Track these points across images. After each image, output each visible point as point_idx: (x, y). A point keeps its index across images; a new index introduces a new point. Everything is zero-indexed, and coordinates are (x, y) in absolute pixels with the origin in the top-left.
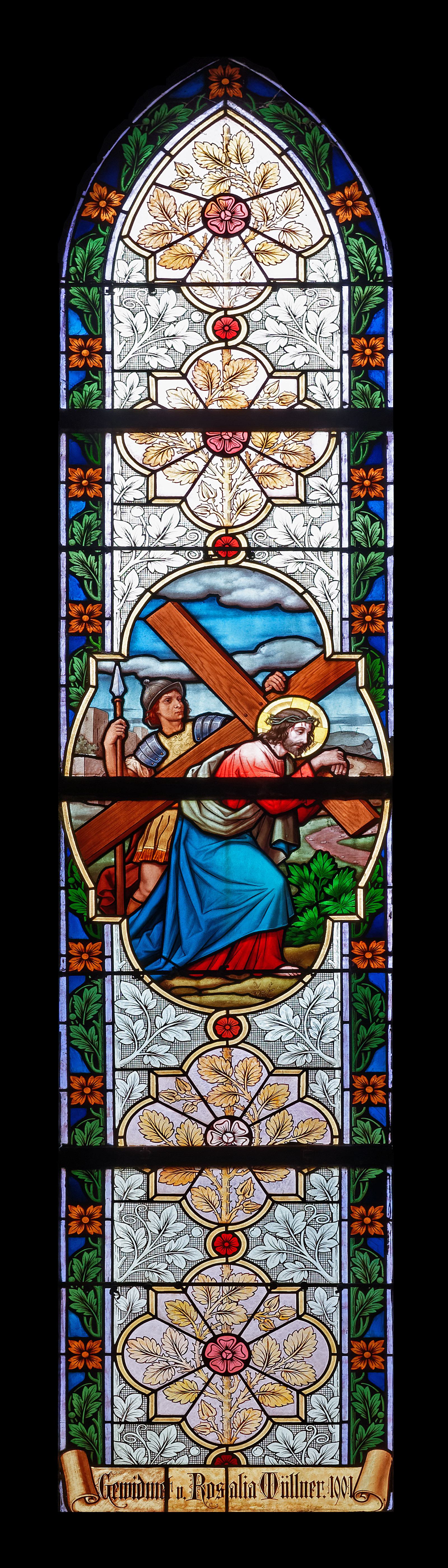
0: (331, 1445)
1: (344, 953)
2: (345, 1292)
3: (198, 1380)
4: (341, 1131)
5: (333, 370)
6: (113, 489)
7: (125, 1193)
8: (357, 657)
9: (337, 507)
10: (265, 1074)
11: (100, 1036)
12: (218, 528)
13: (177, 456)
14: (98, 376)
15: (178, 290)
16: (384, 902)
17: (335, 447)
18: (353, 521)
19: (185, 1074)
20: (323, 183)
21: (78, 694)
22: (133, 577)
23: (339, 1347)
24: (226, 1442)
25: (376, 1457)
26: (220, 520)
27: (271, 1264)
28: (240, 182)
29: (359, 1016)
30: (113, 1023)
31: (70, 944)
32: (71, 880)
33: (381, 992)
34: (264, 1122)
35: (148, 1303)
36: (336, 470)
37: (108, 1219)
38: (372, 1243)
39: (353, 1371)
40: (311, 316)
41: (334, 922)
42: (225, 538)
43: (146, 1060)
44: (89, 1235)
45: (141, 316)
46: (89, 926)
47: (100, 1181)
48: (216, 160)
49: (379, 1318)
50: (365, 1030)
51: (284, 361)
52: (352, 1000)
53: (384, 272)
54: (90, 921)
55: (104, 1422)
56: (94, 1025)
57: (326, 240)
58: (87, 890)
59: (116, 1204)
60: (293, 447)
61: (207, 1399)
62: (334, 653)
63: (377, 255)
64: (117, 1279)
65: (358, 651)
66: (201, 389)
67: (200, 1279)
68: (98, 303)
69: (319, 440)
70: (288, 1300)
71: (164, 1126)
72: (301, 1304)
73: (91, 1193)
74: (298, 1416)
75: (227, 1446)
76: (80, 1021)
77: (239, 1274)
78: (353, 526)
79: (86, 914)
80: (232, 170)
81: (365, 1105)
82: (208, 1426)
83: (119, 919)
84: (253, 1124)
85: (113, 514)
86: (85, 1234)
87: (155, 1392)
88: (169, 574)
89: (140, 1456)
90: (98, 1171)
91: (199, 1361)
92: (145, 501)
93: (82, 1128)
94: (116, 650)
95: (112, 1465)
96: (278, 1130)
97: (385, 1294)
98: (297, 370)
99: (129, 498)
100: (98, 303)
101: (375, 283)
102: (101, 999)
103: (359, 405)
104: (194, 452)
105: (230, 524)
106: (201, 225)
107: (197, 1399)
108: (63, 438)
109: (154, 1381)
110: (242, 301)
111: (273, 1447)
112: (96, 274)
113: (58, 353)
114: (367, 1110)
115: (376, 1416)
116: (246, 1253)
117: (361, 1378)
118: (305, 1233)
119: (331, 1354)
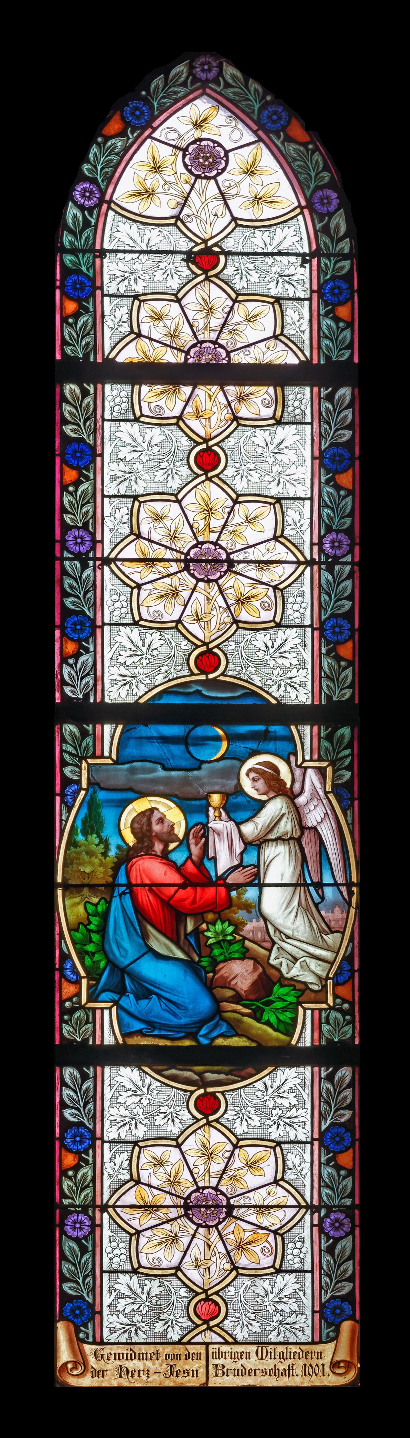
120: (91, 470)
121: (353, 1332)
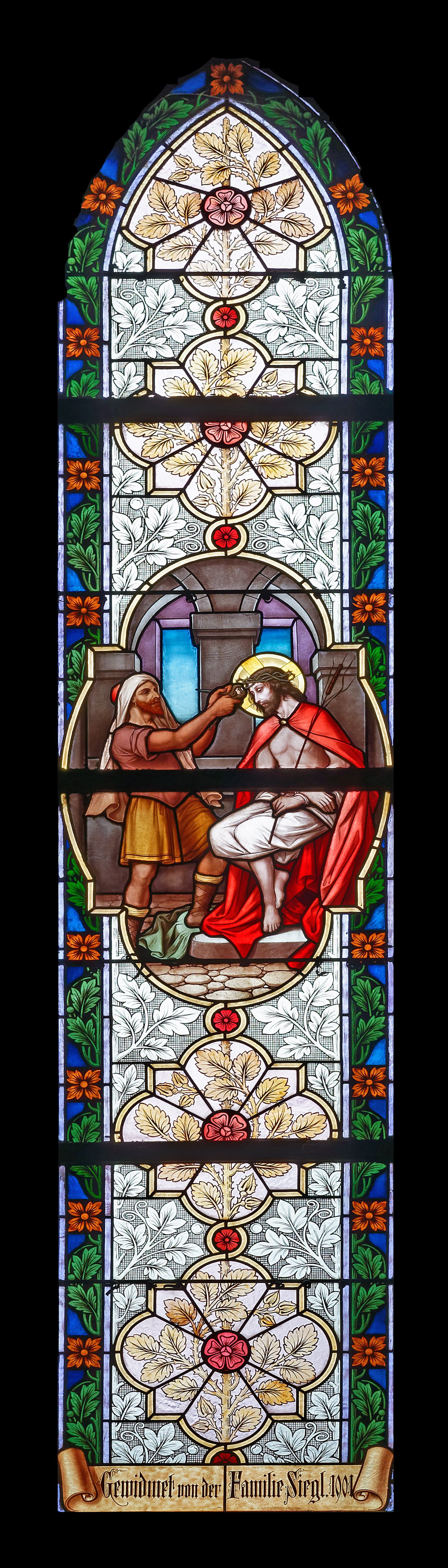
0: (330, 1443)
1: (344, 606)
2: (346, 1289)
3: (196, 1378)
4: (340, 1124)
5: (331, 359)
6: (111, 481)
7: (124, 1189)
8: (357, 646)
9: (337, 497)
10: (263, 1067)
11: (98, 1029)
12: (218, 519)
13: (176, 448)
14: (95, 365)
15: (177, 281)
16: (386, 555)
17: (336, 437)
18: (352, 379)
19: (183, 1068)
20: (324, 177)
21: (77, 687)
22: (132, 569)
23: (340, 1344)
24: (226, 1217)
25: (375, 1455)
26: (218, 1436)
27: (271, 337)
28: (240, 171)
29: (358, 1009)
30: (110, 1017)
31: (70, 1204)
32: (70, 1413)
33: (381, 984)
34: (262, 1116)
35: (147, 1301)
36: (336, 459)
37: (106, 476)
38: (373, 1105)
39: (354, 1098)
40: (311, 305)
41: (333, 914)
42: (224, 528)
43: (144, 1054)
44: (88, 1100)
45: (140, 307)
46: (88, 919)
47: (98, 434)
48: (214, 149)
49: (381, 1045)
50: (364, 1427)
51: (283, 350)
52: (352, 518)
53: (384, 264)
54: (88, 913)
55: (102, 1421)
56: (92, 1018)
57: (327, 231)
58: (85, 882)
59: (115, 1201)
60: (292, 436)
61: (207, 1396)
62: (334, 643)
63: (378, 246)
64: (116, 1277)
65: (359, 641)
66: (199, 1300)
67: (200, 1276)
68: (95, 294)
69: (318, 431)
70: (288, 1296)
71: (162, 1122)
72: (302, 1299)
73: (89, 1057)
74: (297, 1413)
75: (225, 1444)
76: (78, 1014)
77: (238, 1270)
78: (353, 990)
79: (84, 907)
80: (232, 159)
81: (365, 1367)
82: (208, 499)
83: (117, 911)
84: (252, 1118)
85: (111, 507)
86: (84, 1099)
87: (153, 1389)
88: (168, 565)
89: (137, 1454)
90: (97, 1166)
91: (198, 1360)
92: (143, 493)
93: (80, 1255)
94: (114, 642)
95: (110, 1464)
96: (276, 1124)
97: (386, 1291)
98: (297, 1061)
99: (128, 490)
100: (95, 294)
101: (377, 273)
102: (98, 1396)
103: (360, 1136)
104: (192, 444)
105: (229, 515)
106: (200, 217)
107: (196, 1396)
108: (61, 427)
109: (153, 1377)
110: (241, 290)
111: (272, 1445)
112: (94, 265)
113: (57, 1086)
114: (367, 1373)
115: (377, 1009)
116: (247, 1248)
117: (362, 495)
118: (306, 307)
119: (331, 1352)
120: (99, 634)
121: (384, 1461)
